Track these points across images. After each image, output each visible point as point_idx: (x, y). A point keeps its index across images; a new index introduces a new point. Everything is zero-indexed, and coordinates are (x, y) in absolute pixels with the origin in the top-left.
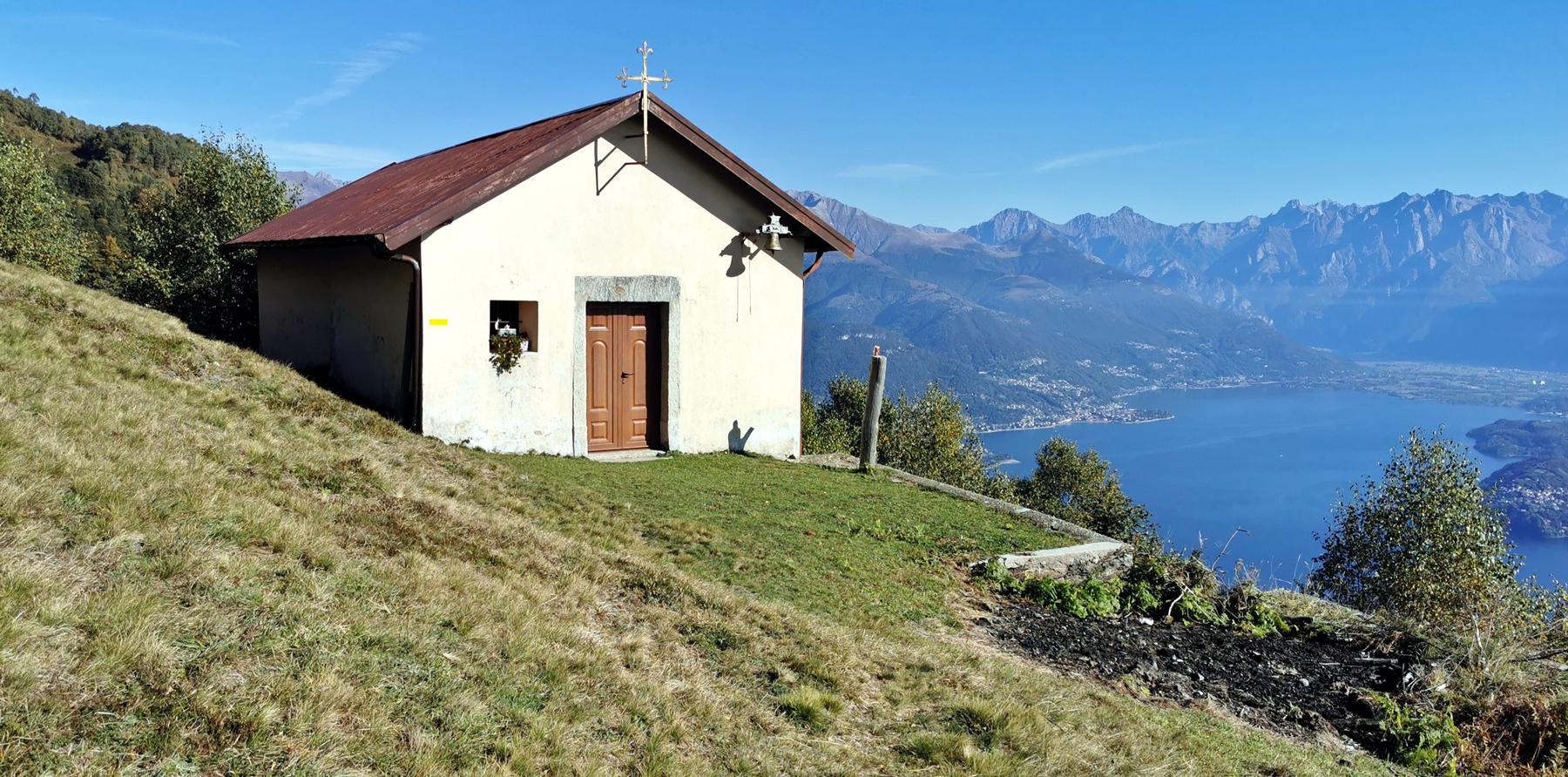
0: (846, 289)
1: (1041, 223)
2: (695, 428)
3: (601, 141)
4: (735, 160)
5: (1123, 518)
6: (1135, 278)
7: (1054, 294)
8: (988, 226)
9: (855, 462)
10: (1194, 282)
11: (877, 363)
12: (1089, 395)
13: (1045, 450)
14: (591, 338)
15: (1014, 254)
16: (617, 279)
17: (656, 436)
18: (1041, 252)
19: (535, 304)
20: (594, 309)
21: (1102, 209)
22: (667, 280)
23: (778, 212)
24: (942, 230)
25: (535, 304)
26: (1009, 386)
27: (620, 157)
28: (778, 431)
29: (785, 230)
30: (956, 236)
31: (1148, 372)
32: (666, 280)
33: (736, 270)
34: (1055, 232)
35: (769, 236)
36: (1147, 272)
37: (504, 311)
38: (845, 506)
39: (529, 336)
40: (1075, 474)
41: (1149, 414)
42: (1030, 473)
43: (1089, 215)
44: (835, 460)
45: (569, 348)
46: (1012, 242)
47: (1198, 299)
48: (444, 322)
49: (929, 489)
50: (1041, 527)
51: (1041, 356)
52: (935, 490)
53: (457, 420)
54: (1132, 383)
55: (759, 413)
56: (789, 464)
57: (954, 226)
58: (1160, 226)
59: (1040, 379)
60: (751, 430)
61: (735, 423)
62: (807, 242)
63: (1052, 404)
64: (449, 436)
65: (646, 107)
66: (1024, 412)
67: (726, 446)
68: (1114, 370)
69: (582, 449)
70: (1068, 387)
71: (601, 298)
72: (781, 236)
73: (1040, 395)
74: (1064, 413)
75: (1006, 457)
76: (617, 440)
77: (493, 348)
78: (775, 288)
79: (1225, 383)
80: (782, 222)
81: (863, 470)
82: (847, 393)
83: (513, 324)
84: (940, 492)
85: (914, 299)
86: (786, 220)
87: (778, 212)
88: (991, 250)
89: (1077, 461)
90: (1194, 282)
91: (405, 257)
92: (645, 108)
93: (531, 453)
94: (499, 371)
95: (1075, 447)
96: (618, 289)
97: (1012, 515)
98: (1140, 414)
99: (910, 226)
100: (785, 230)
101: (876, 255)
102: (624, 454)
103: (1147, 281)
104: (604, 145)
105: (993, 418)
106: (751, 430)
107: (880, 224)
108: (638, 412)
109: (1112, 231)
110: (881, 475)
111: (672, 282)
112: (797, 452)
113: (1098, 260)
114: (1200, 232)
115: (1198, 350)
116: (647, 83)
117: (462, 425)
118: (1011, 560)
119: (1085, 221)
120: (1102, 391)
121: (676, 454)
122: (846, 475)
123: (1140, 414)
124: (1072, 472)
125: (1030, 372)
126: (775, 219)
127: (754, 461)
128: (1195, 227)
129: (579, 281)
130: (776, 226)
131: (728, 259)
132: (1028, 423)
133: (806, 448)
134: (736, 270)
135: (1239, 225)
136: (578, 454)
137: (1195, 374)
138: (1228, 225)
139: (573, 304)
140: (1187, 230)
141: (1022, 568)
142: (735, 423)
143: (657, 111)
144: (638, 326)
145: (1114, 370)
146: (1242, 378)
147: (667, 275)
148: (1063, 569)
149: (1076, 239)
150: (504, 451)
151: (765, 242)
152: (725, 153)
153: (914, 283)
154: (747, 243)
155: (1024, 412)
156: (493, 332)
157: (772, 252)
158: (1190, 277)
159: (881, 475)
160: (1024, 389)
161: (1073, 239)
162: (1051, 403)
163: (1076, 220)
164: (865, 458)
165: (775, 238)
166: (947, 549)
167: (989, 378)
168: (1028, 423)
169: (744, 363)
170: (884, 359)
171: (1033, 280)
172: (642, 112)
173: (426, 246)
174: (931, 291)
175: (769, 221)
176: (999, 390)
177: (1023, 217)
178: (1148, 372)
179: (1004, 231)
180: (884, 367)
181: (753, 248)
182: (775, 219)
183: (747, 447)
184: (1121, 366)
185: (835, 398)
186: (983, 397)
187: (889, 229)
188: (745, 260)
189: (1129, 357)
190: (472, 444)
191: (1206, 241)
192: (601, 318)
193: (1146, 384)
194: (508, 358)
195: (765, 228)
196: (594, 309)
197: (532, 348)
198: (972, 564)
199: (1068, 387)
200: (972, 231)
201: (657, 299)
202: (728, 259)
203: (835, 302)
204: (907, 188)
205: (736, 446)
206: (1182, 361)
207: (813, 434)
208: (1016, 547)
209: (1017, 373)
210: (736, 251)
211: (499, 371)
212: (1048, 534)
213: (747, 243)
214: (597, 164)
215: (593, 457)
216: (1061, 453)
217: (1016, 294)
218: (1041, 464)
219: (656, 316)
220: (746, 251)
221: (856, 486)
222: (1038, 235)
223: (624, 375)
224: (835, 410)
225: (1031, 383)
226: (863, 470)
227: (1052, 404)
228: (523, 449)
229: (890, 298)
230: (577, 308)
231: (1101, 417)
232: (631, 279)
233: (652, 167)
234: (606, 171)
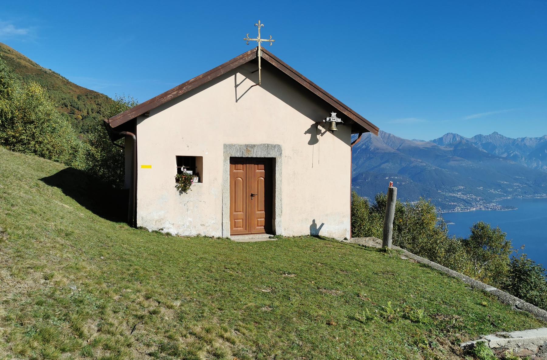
0: (387, 161)
1: (462, 138)
2: (291, 222)
3: (238, 74)
4: (311, 84)
5: (530, 271)
6: (500, 158)
7: (467, 163)
8: (441, 139)
9: (378, 243)
10: (523, 159)
11: (391, 191)
12: (482, 200)
13: (475, 227)
14: (233, 177)
15: (452, 149)
16: (247, 146)
17: (270, 228)
18: (462, 149)
19: (202, 157)
20: (234, 161)
21: (486, 132)
22: (276, 145)
23: (335, 110)
24: (423, 141)
25: (202, 157)
26: (450, 196)
27: (249, 83)
28: (337, 225)
29: (339, 120)
30: (428, 143)
31: (506, 192)
32: (275, 146)
33: (313, 141)
34: (467, 141)
35: (330, 123)
36: (505, 155)
37: (182, 161)
38: (367, 282)
39: (198, 174)
40: (490, 238)
41: (507, 208)
42: (468, 235)
43: (480, 135)
44: (369, 242)
45: (220, 181)
46: (450, 145)
47: (525, 165)
48: (150, 167)
49: (424, 266)
50: (508, 305)
51: (462, 186)
52: (428, 266)
53: (156, 218)
54: (500, 196)
55: (327, 215)
56: (342, 244)
57: (427, 140)
58: (509, 139)
59: (463, 194)
60: (323, 224)
61: (314, 221)
62: (352, 127)
63: (467, 203)
64: (151, 227)
65: (260, 54)
66: (456, 206)
67: (308, 232)
68: (492, 191)
69: (227, 234)
70: (474, 197)
71: (238, 155)
72: (337, 124)
73: (463, 200)
74: (473, 206)
75: (449, 222)
76: (249, 230)
77: (177, 180)
78: (335, 152)
79: (538, 196)
80: (338, 116)
81: (383, 250)
82: (383, 201)
83: (189, 167)
84: (432, 269)
85: (412, 165)
86: (339, 115)
87: (335, 110)
88: (442, 148)
89: (491, 232)
90: (523, 159)
91: (128, 133)
92: (259, 56)
93: (198, 236)
94: (181, 192)
95: (490, 226)
96: (247, 150)
97: (485, 293)
98: (503, 207)
99: (410, 139)
100: (339, 120)
101: (398, 149)
102: (251, 236)
103: (505, 159)
104: (240, 77)
105: (444, 207)
106: (323, 224)
107: (399, 139)
108: (260, 214)
109: (490, 141)
110: (395, 254)
111: (278, 148)
112: (348, 236)
113: (485, 151)
114: (525, 141)
115: (526, 184)
116: (260, 43)
117: (160, 221)
118: (494, 340)
119: (479, 137)
120: (488, 199)
121: (279, 237)
122: (374, 254)
123: (503, 207)
124: (488, 237)
125: (458, 191)
126: (334, 114)
127: (322, 243)
128: (523, 139)
129: (225, 146)
130: (334, 118)
131: (309, 136)
132: (458, 210)
133: (354, 234)
134: (313, 141)
135: (541, 139)
136: (225, 237)
137: (525, 193)
138: (537, 138)
139: (223, 158)
140: (520, 140)
141: (505, 348)
142: (314, 221)
143: (266, 57)
144: (258, 172)
145: (492, 191)
146: (545, 195)
147: (275, 143)
148: (535, 349)
149: (475, 143)
150: (183, 235)
151: (328, 126)
152: (305, 80)
153: (413, 159)
154: (320, 127)
155: (456, 206)
156: (179, 171)
157: (333, 132)
158: (522, 157)
159: (395, 254)
160: (456, 197)
161: (475, 143)
162: (467, 202)
163: (475, 137)
164: (385, 243)
165: (334, 124)
166: (444, 328)
167: (442, 193)
168: (458, 210)
169: (318, 189)
170: (395, 189)
171: (459, 158)
172: (258, 57)
173: (140, 127)
174: (419, 162)
175: (330, 116)
176: (446, 197)
177: (454, 136)
178: (506, 192)
179: (447, 141)
180: (395, 193)
181: (323, 130)
182: (334, 114)
183: (321, 234)
184: (495, 189)
185: (378, 202)
186: (440, 200)
187: (402, 141)
188: (319, 137)
189: (498, 186)
190: (165, 231)
191: (528, 144)
192: (240, 166)
193: (505, 196)
194: (185, 186)
195: (328, 119)
196: (234, 161)
197: (200, 181)
198: (463, 344)
199: (474, 197)
200: (435, 141)
201: (269, 156)
202: (309, 136)
203: (383, 166)
204: (408, 123)
205: (314, 232)
206: (520, 188)
207: (357, 227)
208: (496, 326)
209: (453, 191)
210: (314, 132)
211: (181, 192)
212: (516, 313)
213: (320, 127)
214: (236, 86)
215: (233, 238)
216: (483, 228)
217: (452, 163)
218: (473, 232)
219: (269, 164)
220: (319, 132)
221: (378, 263)
222: (460, 142)
223: (252, 195)
224: (370, 210)
225: (459, 195)
226: (383, 250)
227: (467, 203)
228: (194, 233)
229: (404, 165)
230: (225, 161)
231: (488, 208)
232: (254, 146)
233: (263, 86)
234: (241, 90)
